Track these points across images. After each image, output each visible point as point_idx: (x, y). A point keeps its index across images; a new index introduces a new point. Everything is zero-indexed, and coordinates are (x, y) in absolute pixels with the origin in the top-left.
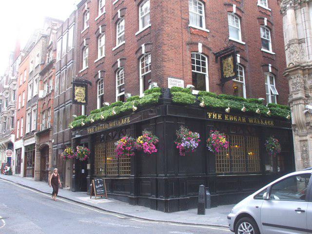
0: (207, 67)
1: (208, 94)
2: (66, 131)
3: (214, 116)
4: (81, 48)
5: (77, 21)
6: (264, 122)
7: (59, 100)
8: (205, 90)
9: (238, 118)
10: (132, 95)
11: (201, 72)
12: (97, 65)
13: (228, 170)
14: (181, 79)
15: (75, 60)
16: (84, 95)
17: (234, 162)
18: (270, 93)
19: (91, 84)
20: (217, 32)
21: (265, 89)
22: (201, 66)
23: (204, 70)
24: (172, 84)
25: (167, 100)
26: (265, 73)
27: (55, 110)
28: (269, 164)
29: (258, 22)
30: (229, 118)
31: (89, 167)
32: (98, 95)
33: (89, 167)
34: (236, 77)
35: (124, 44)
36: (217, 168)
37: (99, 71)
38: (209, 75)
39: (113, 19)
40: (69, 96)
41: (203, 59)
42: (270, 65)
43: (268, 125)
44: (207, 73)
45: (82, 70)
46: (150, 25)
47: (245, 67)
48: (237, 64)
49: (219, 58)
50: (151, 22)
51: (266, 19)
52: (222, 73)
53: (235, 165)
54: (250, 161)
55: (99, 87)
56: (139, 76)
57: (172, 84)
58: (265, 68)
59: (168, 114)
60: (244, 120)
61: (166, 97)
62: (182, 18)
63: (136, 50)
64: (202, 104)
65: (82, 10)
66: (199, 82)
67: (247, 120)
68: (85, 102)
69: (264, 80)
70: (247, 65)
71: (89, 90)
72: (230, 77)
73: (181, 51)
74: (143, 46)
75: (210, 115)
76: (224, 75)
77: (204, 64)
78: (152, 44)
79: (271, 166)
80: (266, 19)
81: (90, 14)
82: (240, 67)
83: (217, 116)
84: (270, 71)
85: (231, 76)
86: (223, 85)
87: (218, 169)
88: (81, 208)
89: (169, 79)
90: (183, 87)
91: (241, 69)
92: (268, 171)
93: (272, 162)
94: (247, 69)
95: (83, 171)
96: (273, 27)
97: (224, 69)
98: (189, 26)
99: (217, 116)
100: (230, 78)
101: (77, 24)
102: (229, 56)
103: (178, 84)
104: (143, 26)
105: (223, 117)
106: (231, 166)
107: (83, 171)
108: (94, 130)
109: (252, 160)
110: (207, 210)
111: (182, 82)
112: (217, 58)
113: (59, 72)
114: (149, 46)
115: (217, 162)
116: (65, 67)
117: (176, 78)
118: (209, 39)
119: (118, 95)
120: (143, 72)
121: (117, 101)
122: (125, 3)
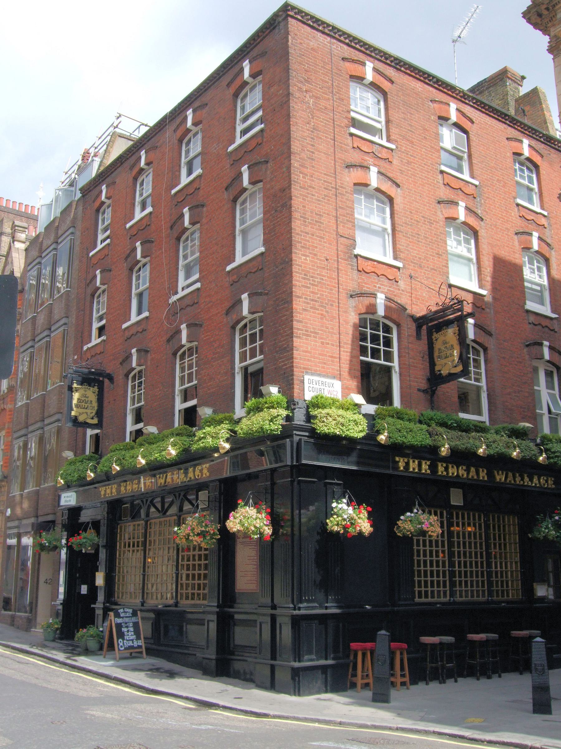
0: (394, 336)
1: (399, 415)
2: (45, 489)
3: (413, 465)
4: (89, 291)
5: (79, 225)
6: (531, 480)
7: (27, 411)
8: (391, 404)
9: (468, 471)
10: (214, 412)
11: (382, 362)
12: (127, 334)
13: (445, 593)
14: (334, 378)
15: (73, 319)
16: (95, 405)
17: (460, 576)
18: (545, 411)
19: (111, 378)
20: (420, 267)
21: (533, 400)
22: (382, 348)
23: (388, 356)
24: (313, 390)
25: (300, 428)
26: (535, 363)
27: (15, 435)
28: (544, 580)
29: (516, 243)
30: (446, 469)
31: (100, 580)
32: (129, 407)
33: (100, 580)
34: (465, 373)
35: (198, 289)
36: (417, 589)
37: (134, 351)
38: (400, 368)
39: (172, 228)
40: (53, 403)
41: (387, 329)
42: (546, 343)
43: (541, 487)
44: (395, 364)
45: (90, 345)
46: (262, 249)
47: (485, 349)
48: (468, 342)
49: (424, 327)
50: (266, 242)
51: (535, 235)
52: (432, 364)
53: (460, 582)
54: (496, 572)
55: (133, 387)
56: (233, 368)
57: (313, 390)
58: (535, 349)
59: (304, 462)
60: (483, 475)
61: (299, 418)
62: (337, 233)
63: (227, 305)
64: (382, 438)
65: (94, 202)
66: (376, 383)
67: (490, 475)
68: (95, 421)
69: (534, 381)
70: (491, 343)
71: (106, 395)
72: (450, 375)
73: (335, 313)
74: (245, 296)
75: (401, 465)
76: (437, 368)
77: (388, 343)
78: (267, 294)
79: (549, 586)
80: (535, 235)
81: (114, 211)
82: (473, 347)
83: (420, 465)
84: (547, 356)
85: (454, 371)
86: (433, 393)
87: (420, 592)
88: (85, 683)
89: (306, 378)
90: (339, 396)
91: (477, 352)
92: (542, 599)
93: (551, 575)
94: (490, 353)
95: (84, 589)
96: (553, 252)
97: (436, 354)
98: (356, 252)
99: (420, 465)
100: (452, 377)
101: (78, 233)
102: (448, 323)
103: (327, 389)
104: (243, 255)
105: (434, 467)
106: (453, 584)
107: (84, 589)
108: (118, 491)
109: (502, 572)
110: (393, 693)
111: (338, 385)
112: (419, 328)
113: (30, 344)
114: (260, 300)
115: (419, 576)
116: (46, 333)
117: (324, 376)
118: (401, 283)
119: (179, 406)
120: (243, 358)
121: (176, 425)
122: (201, 192)
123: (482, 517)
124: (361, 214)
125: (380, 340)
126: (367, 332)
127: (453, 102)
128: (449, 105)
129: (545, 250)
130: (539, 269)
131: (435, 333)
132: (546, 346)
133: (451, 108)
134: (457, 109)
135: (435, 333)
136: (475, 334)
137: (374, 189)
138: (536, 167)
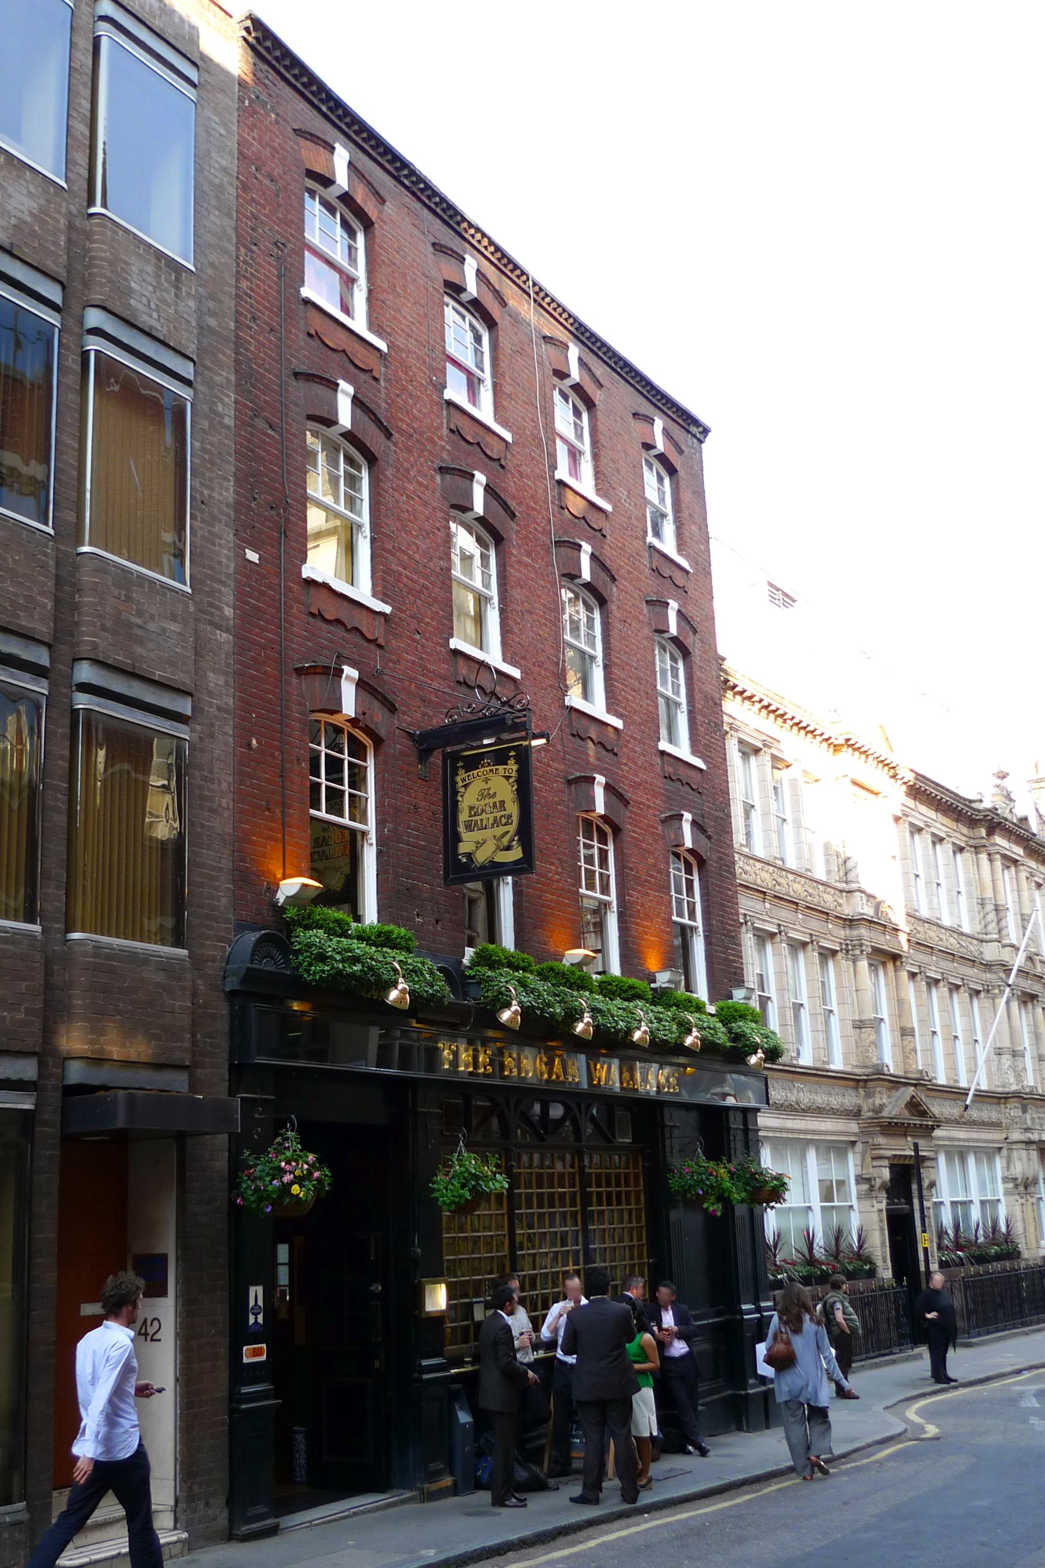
0: (370, 764)
42: (600, 779)
51: (346, 388)
76: (464, 848)
77: (357, 780)
123: (640, 1159)
124: (316, 490)
125: (342, 771)
126: (320, 752)
127: (661, 419)
128: (332, 149)
129: (499, 519)
130: (352, 481)
131: (461, 772)
132: (599, 783)
133: (336, 157)
134: (580, 359)
135: (461, 772)
136: (606, 804)
137: (476, 519)
138: (590, 405)
